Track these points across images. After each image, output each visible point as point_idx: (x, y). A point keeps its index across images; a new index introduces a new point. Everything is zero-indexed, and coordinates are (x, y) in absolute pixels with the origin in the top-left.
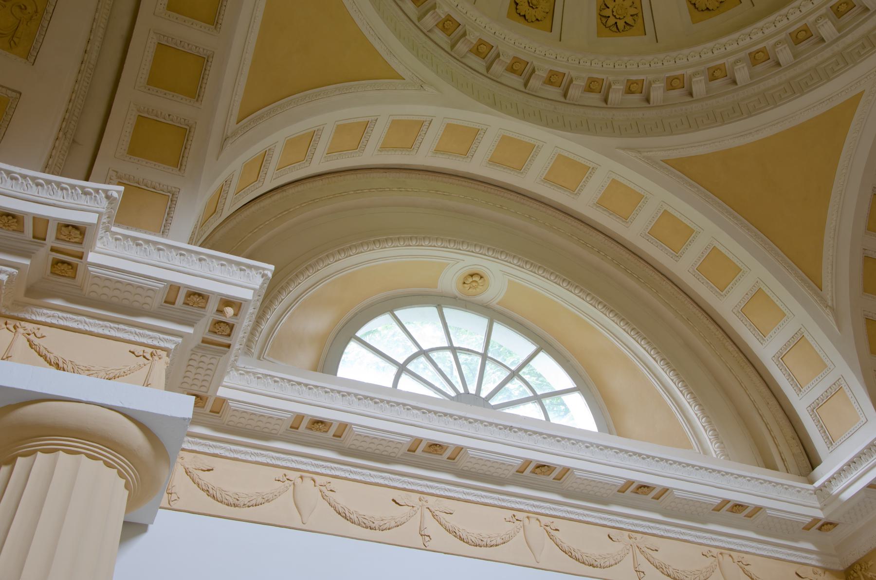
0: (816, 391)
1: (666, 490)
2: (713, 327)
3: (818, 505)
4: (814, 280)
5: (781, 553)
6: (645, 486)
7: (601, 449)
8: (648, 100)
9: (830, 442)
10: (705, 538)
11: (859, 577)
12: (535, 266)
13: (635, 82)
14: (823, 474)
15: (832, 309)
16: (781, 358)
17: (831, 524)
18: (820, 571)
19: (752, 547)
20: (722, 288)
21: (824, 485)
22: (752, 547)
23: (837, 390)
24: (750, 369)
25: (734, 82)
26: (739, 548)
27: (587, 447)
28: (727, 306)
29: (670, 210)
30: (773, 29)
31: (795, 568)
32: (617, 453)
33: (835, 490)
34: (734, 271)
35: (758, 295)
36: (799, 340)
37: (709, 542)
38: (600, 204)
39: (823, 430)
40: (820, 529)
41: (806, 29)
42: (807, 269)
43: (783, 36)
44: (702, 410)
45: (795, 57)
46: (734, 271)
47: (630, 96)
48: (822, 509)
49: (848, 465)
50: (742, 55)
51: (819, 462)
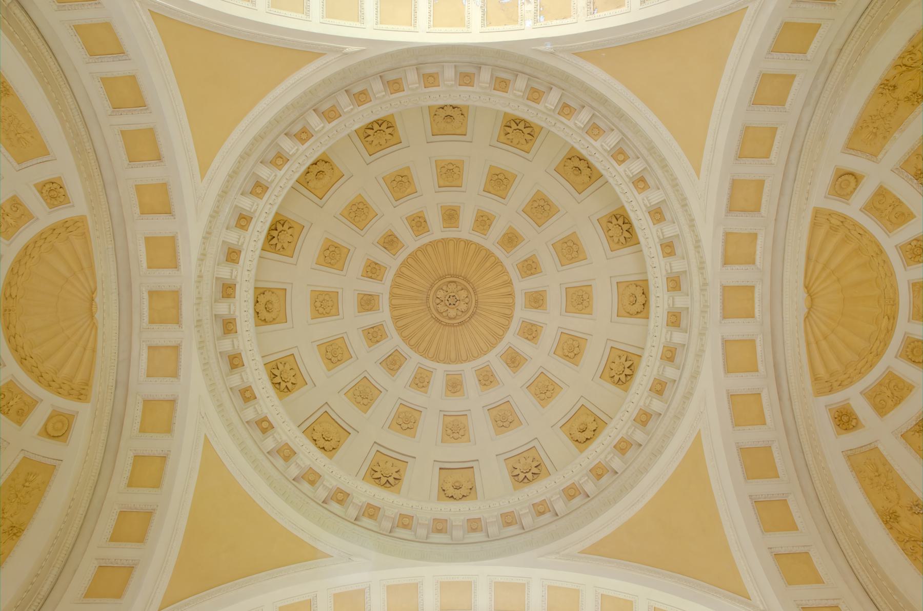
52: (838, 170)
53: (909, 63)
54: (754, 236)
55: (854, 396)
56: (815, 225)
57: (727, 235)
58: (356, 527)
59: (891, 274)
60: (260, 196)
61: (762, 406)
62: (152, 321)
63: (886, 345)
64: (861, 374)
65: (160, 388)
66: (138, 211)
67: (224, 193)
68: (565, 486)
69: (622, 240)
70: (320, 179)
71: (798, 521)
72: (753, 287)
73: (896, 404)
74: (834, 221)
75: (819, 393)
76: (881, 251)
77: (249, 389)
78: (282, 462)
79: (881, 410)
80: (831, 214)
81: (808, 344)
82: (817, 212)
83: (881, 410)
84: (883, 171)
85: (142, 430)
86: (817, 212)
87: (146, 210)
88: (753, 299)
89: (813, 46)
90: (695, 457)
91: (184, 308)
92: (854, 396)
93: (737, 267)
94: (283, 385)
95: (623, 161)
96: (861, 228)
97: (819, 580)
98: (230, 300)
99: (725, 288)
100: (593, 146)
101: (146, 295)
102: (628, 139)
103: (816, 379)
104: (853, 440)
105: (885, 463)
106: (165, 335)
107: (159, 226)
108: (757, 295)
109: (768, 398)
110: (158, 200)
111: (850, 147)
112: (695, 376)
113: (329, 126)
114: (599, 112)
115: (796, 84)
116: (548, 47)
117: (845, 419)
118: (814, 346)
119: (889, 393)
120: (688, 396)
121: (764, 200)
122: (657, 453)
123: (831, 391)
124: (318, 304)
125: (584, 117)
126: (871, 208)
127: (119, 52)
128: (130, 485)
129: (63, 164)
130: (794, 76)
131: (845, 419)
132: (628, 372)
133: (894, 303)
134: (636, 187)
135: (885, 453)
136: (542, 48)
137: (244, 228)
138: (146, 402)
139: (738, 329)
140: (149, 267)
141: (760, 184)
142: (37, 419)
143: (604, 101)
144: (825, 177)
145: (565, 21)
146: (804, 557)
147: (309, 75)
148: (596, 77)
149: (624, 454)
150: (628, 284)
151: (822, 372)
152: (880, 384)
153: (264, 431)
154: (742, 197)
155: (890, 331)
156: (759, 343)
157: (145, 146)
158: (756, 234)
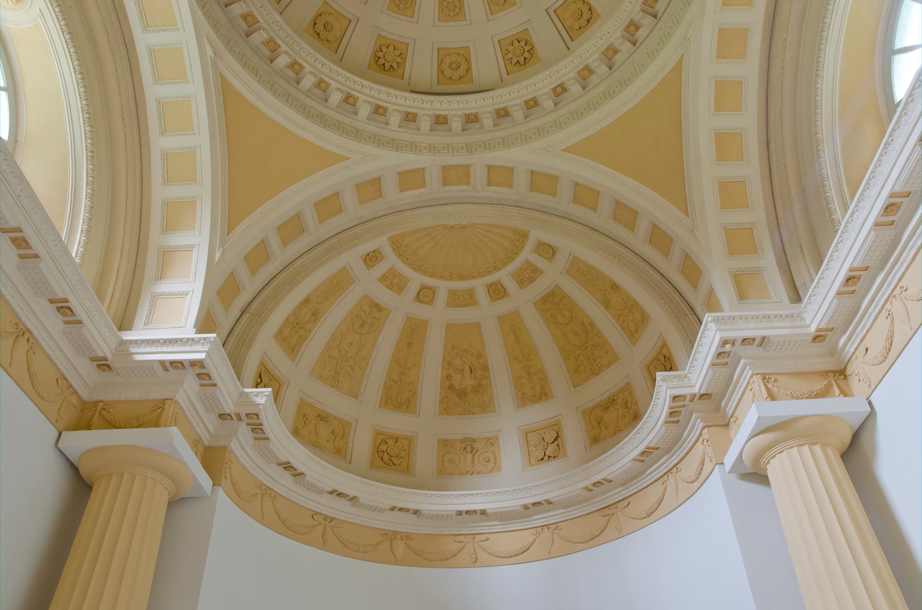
14: (128, 336)
17: (109, 367)
21: (132, 342)
33: (133, 350)
55: (392, 261)
58: (664, 18)
60: (356, 99)
62: (468, 183)
65: (522, 180)
66: (380, 199)
67: (357, 134)
70: (332, 27)
77: (526, 103)
78: (593, 77)
79: (383, 279)
84: (553, 275)
85: (554, 195)
87: (379, 194)
91: (456, 163)
94: (527, 55)
98: (449, 119)
99: (467, 167)
101: (447, 188)
106: (479, 175)
107: (390, 185)
110: (371, 188)
112: (395, 145)
113: (284, 47)
120: (376, 140)
124: (451, 13)
127: (263, 244)
128: (595, 210)
129: (351, 258)
132: (387, 66)
137: (385, 110)
138: (532, 190)
140: (424, 187)
147: (243, 83)
153: (565, 90)
154: (542, 181)
157: (328, 205)
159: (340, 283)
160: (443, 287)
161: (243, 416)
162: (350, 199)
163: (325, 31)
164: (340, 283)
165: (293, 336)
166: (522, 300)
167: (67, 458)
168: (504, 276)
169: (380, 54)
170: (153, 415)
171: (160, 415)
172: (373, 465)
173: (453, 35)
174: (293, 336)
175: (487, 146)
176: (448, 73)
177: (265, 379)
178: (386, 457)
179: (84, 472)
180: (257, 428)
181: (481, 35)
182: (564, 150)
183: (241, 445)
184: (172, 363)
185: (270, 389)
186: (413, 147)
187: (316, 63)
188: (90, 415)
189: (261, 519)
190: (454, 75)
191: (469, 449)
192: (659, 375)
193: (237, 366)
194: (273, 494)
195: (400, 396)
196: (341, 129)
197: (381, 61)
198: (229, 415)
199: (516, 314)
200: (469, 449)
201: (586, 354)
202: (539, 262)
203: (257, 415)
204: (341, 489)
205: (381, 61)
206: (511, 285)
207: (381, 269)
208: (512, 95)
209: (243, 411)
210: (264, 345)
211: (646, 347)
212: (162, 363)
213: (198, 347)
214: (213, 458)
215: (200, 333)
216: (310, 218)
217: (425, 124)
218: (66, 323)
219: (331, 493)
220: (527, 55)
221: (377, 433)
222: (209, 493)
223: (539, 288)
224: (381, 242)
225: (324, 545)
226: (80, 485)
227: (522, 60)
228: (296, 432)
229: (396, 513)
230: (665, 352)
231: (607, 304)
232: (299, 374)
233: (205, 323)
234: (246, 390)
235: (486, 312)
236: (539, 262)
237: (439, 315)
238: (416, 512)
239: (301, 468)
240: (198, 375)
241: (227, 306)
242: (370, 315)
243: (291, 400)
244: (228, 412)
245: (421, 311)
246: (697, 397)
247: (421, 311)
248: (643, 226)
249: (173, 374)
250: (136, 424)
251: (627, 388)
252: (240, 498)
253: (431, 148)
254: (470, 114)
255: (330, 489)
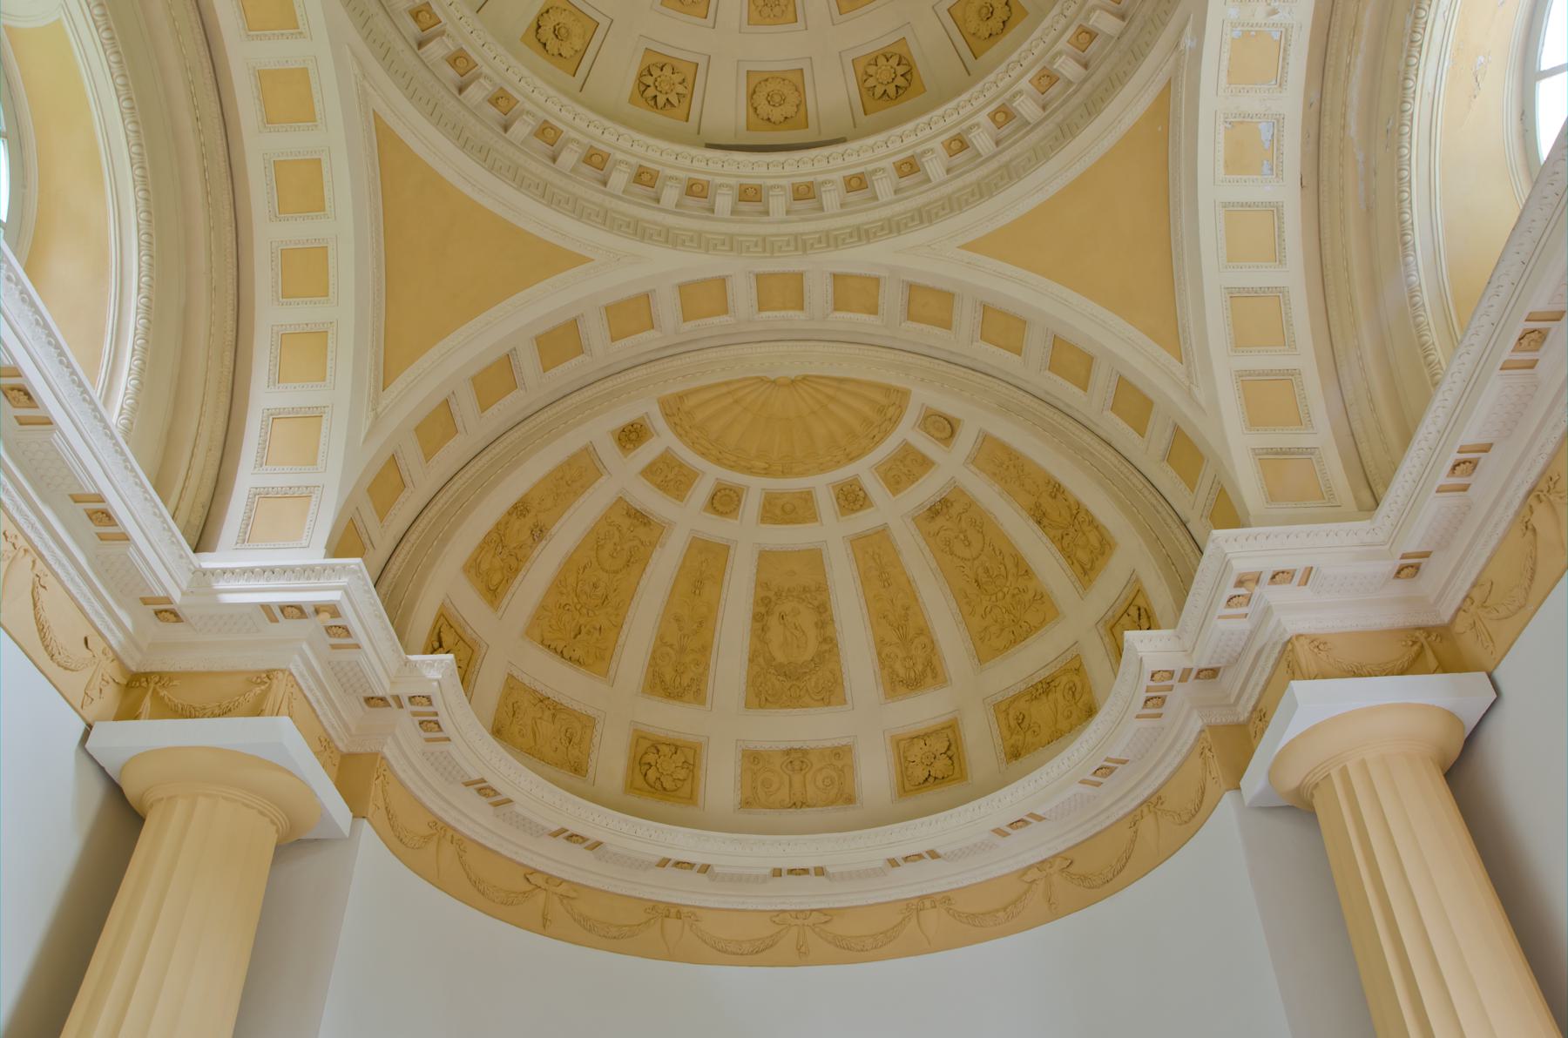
0: (279, 479)
1: (48, 422)
2: (230, 323)
3: (184, 586)
4: (387, 376)
5: (92, 607)
6: (27, 394)
7: (23, 300)
8: (420, 45)
9: (245, 539)
10: (26, 519)
11: (147, 689)
12: (114, 45)
13: (432, 15)
14: (208, 561)
15: (377, 417)
16: (275, 417)
17: (176, 615)
18: (111, 655)
19: (66, 572)
20: (287, 293)
21: (213, 572)
22: (66, 572)
23: (303, 496)
24: (225, 400)
25: (506, 129)
26: (52, 562)
27: (9, 278)
28: (272, 315)
29: (325, 166)
30: (584, 125)
31: (90, 632)
32: (37, 323)
34: (320, 289)
35: (317, 338)
36: (312, 417)
37: (25, 526)
38: (263, 77)
39: (248, 522)
40: (157, 613)
41: (605, 158)
42: (391, 358)
43: (586, 140)
44: (138, 390)
45: (573, 170)
46: (320, 289)
47: (410, 20)
48: (183, 594)
49: (244, 571)
50: (540, 114)
51: (212, 550)
52: (959, 421)
53: (1080, 517)
54: (873, 310)
55: (663, 440)
56: (887, 390)
57: (877, 280)
59: (822, 469)
61: (637, 332)
63: (731, 467)
64: (693, 445)
65: (892, 299)
67: (606, 219)
68: (470, 51)
69: (871, 82)
71: (493, 410)
72: (802, 308)
73: (659, 487)
74: (891, 411)
75: (663, 403)
76: (851, 459)
79: (649, 472)
80: (901, 409)
81: (727, 384)
82: (904, 394)
83: (649, 472)
84: (951, 467)
86: (904, 394)
88: (785, 308)
89: (1118, 420)
90: (557, 260)
92: (663, 440)
93: (830, 290)
95: (993, 120)
96: (882, 439)
97: (428, 456)
99: (800, 276)
100: (1021, 76)
102: (1028, 133)
103: (681, 397)
104: (608, 451)
105: (585, 488)
106: (818, 292)
108: (791, 313)
109: (648, 340)
110: (631, 313)
111: (985, 439)
112: (669, 238)
114: (1075, 92)
115: (1076, 390)
116: (1188, 42)
117: (633, 436)
118: (725, 390)
119: (671, 476)
120: (639, 231)
121: (923, 326)
122: (546, 194)
123: (667, 415)
125: (1068, 68)
126: (907, 451)
130: (1085, 389)
131: (633, 436)
132: (661, 100)
133: (784, 473)
134: (954, 139)
135: (596, 485)
136: (1189, 29)
139: (743, 295)
141: (947, 324)
142: (701, 492)
143: (1092, 108)
144: (948, 405)
145: (1224, 74)
146: (451, 430)
148: (1128, 107)
149: (536, 135)
150: (799, 90)
151: (690, 402)
152: (681, 465)
154: (931, 304)
155: (750, 470)
156: (724, 319)
157: (560, 341)
158: (876, 313)
159: (576, 475)
160: (756, 488)
161: (405, 701)
162: (595, 332)
163: (556, 38)
164: (576, 475)
165: (496, 567)
166: (893, 511)
167: (102, 769)
168: (863, 470)
169: (649, 80)
170: (252, 695)
171: (265, 694)
172: (631, 787)
173: (775, 48)
174: (496, 567)
175: (831, 240)
176: (764, 109)
177: (448, 639)
178: (652, 774)
179: (131, 790)
180: (431, 725)
181: (823, 55)
182: (966, 247)
183: (401, 745)
184: (283, 608)
185: (451, 656)
186: (700, 242)
187: (538, 90)
188: (139, 691)
189: (438, 881)
190: (777, 120)
191: (797, 764)
192: (1132, 637)
193: (397, 609)
194: (457, 837)
195: (677, 675)
196: (576, 209)
197: (651, 92)
198: (382, 699)
199: (883, 532)
200: (797, 764)
201: (1003, 604)
202: (926, 445)
203: (429, 699)
204: (575, 828)
205: (651, 92)
206: (874, 487)
207: (647, 453)
208: (875, 152)
209: (405, 691)
210: (445, 584)
211: (1109, 588)
212: (266, 607)
213: (335, 582)
214: (355, 773)
215: (335, 556)
216: (528, 362)
217: (724, 202)
218: (102, 537)
219: (555, 834)
220: (900, 81)
221: (639, 737)
222: (346, 832)
223: (926, 490)
224: (644, 407)
225: (544, 926)
226: (121, 817)
227: (891, 90)
228: (497, 732)
229: (670, 871)
230: (1140, 602)
231: (1040, 517)
232: (506, 636)
233: (346, 542)
234: (413, 658)
235: (831, 533)
236: (926, 445)
237: (747, 536)
238: (705, 869)
239: (506, 791)
240: (328, 629)
241: (382, 512)
242: (631, 531)
243: (490, 680)
244: (380, 694)
245: (717, 528)
246: (1194, 674)
247: (717, 528)
248: (1102, 380)
249: (287, 626)
250: (217, 711)
251: (1076, 667)
252: (399, 840)
253: (732, 244)
254: (801, 184)
255: (555, 828)
